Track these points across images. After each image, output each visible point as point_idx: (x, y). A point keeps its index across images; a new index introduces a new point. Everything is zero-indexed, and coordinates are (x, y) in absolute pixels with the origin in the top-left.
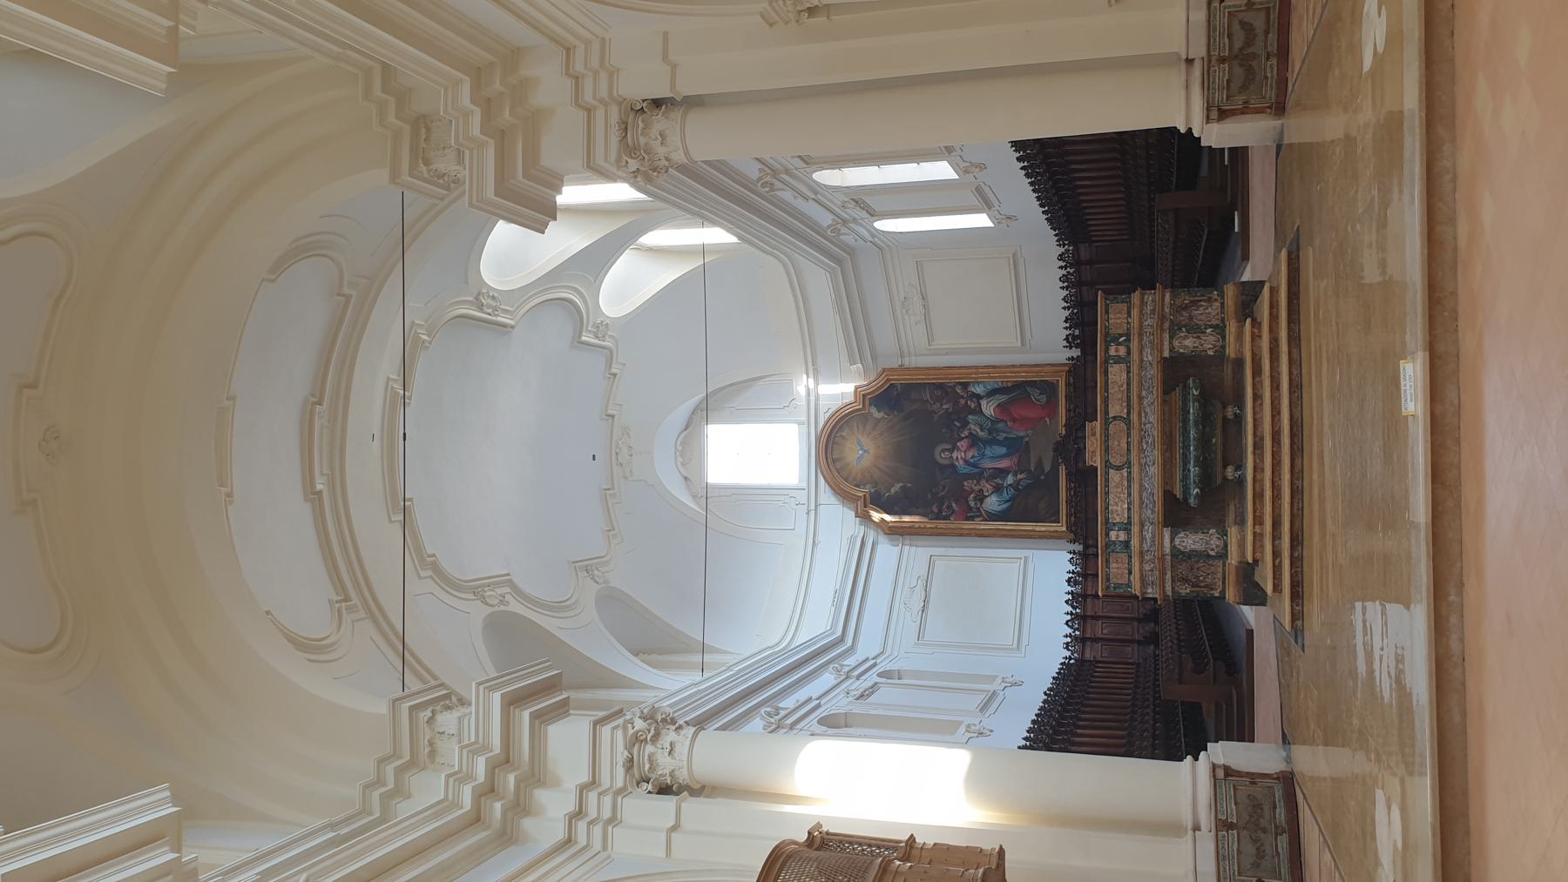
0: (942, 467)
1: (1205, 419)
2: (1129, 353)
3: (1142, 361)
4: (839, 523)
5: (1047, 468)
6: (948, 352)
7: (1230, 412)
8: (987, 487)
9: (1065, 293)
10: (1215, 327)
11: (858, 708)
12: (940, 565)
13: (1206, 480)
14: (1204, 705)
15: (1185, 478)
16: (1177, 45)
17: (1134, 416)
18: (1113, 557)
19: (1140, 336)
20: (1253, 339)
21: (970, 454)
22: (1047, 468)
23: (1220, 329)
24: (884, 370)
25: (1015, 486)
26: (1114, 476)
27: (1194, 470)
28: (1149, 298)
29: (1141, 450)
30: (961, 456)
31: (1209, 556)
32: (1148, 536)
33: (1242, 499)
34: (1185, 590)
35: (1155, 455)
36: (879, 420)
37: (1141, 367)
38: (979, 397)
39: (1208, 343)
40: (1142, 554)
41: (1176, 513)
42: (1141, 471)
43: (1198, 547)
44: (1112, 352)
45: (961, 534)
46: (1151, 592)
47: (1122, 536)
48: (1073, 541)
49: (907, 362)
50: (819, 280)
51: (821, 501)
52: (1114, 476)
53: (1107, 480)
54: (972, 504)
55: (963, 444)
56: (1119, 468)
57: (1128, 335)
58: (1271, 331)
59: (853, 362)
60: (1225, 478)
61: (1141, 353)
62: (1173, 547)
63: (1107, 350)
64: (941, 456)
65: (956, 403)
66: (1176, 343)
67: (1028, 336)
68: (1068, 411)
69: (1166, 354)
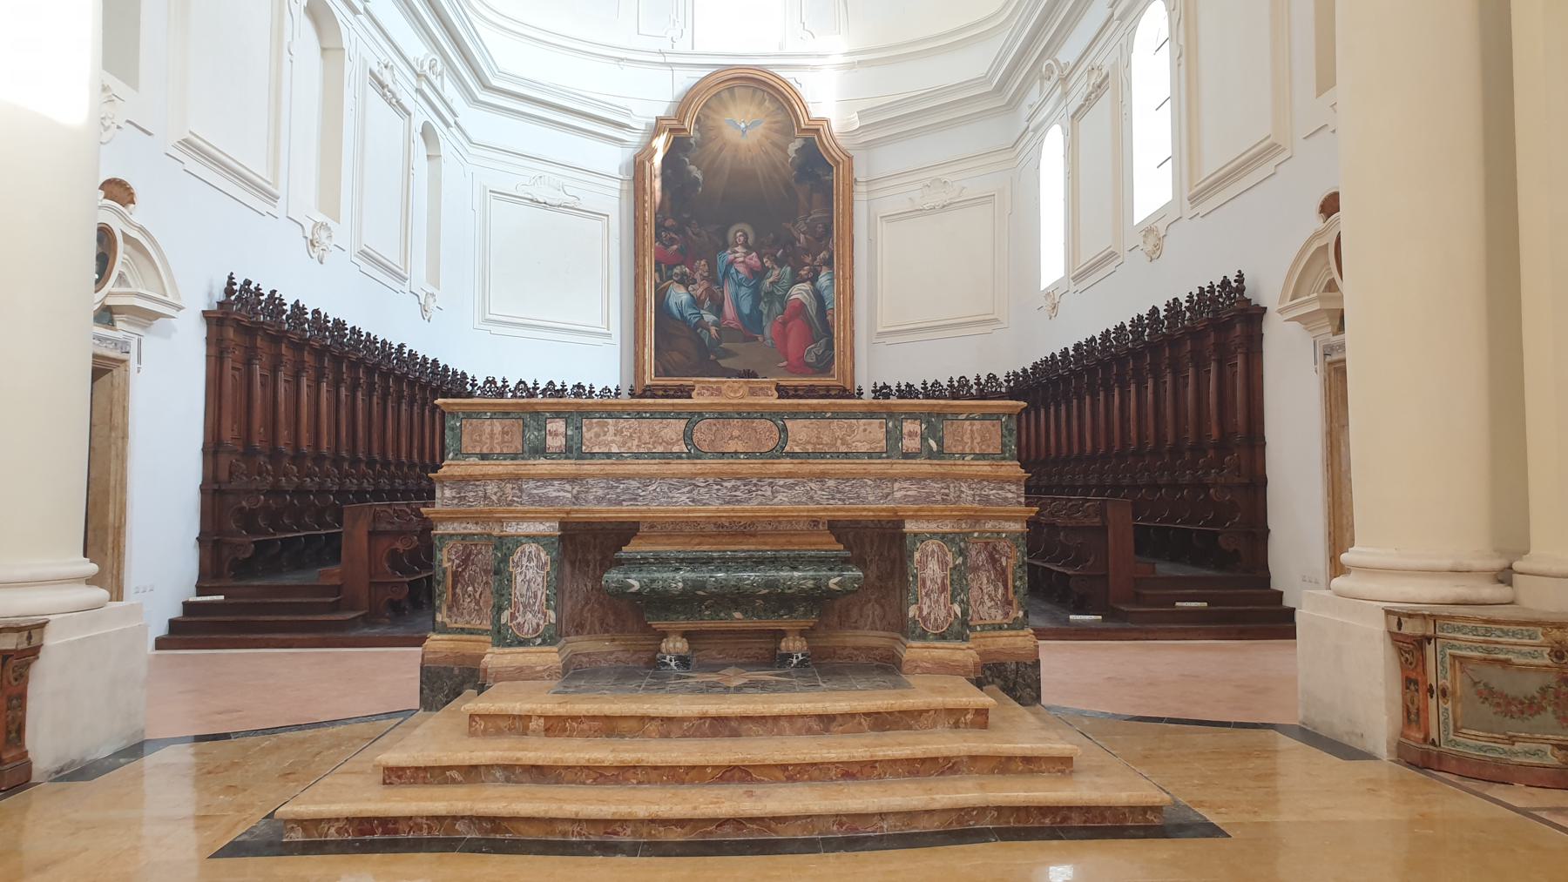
0: (723, 233)
1: (781, 600)
2: (907, 456)
3: (894, 479)
4: (650, 96)
6: (872, 241)
7: (794, 646)
8: (699, 289)
9: (945, 384)
10: (965, 622)
11: (353, 72)
12: (597, 226)
13: (659, 602)
14: (336, 569)
15: (662, 561)
16: (1550, 548)
17: (785, 465)
18: (514, 425)
19: (943, 477)
20: (950, 711)
21: (741, 268)
22: (724, 363)
23: (961, 630)
24: (850, 158)
25: (701, 324)
26: (673, 430)
27: (677, 579)
28: (1014, 493)
29: (721, 478)
30: (739, 257)
31: (499, 609)
32: (551, 491)
33: (624, 675)
34: (446, 559)
35: (712, 505)
36: (784, 150)
37: (881, 478)
38: (814, 280)
39: (930, 607)
40: (516, 478)
41: (588, 545)
42: (681, 477)
43: (519, 587)
44: (909, 426)
46: (444, 494)
47: (555, 443)
49: (860, 189)
50: (974, 65)
51: (679, 72)
52: (673, 430)
53: (664, 415)
56: (688, 436)
57: (941, 454)
58: (974, 758)
59: (862, 114)
60: (664, 635)
61: (910, 478)
62: (518, 541)
63: (912, 416)
64: (737, 232)
65: (807, 251)
66: (932, 545)
67: (889, 340)
69: (910, 527)
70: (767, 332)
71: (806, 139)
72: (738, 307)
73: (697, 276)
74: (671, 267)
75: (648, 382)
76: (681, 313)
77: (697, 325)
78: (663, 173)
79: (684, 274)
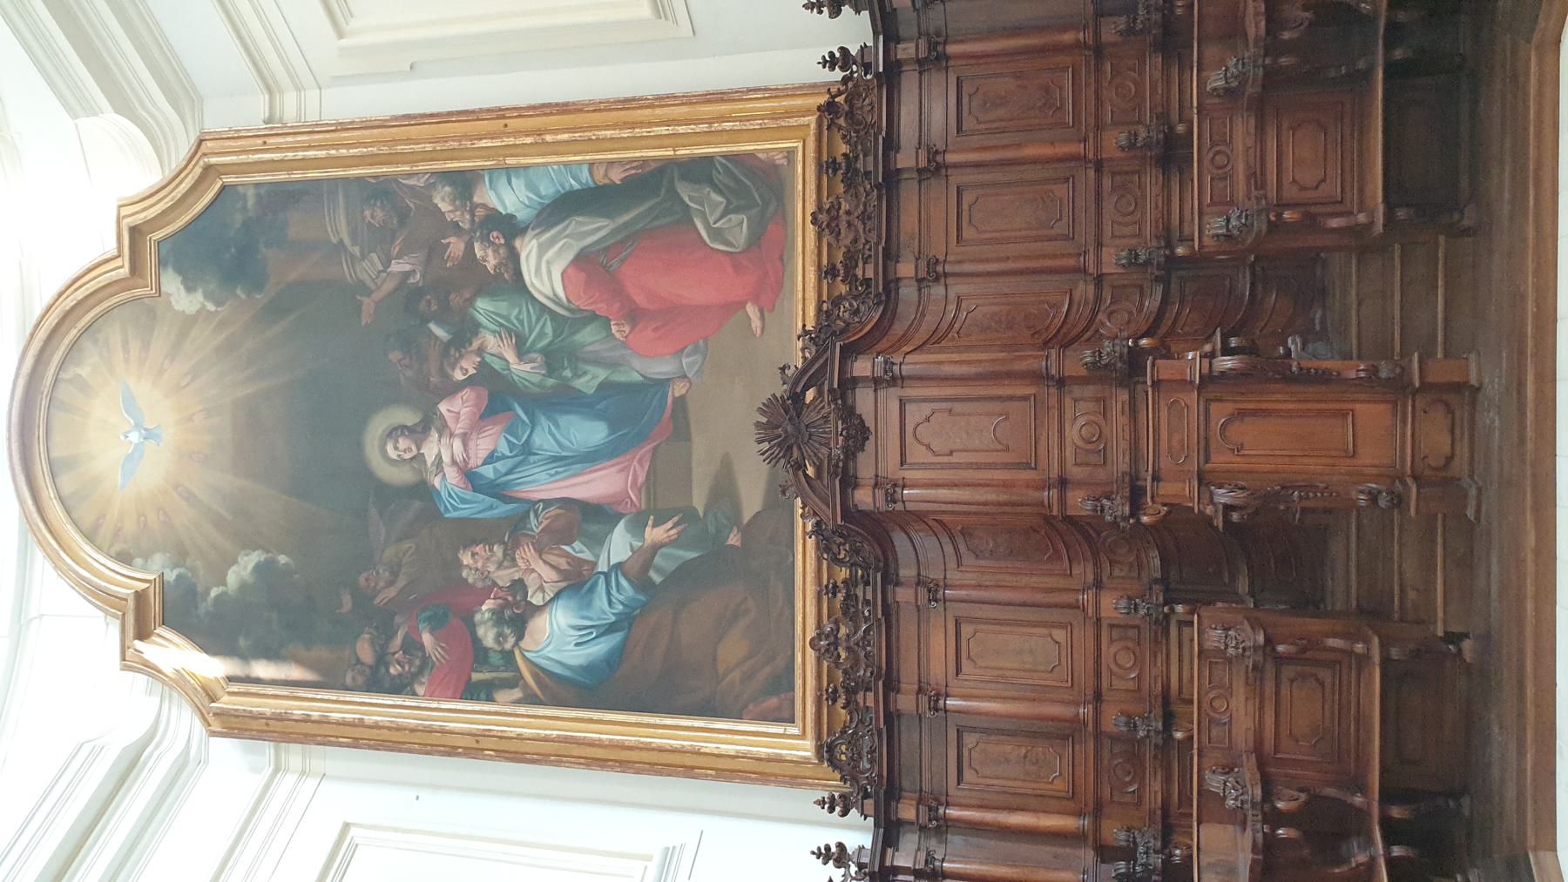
0: (387, 495)
5: (732, 184)
8: (540, 574)
21: (482, 446)
25: (638, 570)
38: (510, 228)
45: (474, 748)
48: (839, 804)
49: (290, 110)
54: (487, 635)
55: (457, 409)
64: (387, 455)
65: (434, 250)
68: (827, 273)
70: (660, 368)
71: (161, 263)
72: (591, 458)
73: (504, 577)
74: (480, 655)
75: (805, 749)
76: (610, 629)
77: (642, 583)
78: (245, 656)
79: (498, 617)
